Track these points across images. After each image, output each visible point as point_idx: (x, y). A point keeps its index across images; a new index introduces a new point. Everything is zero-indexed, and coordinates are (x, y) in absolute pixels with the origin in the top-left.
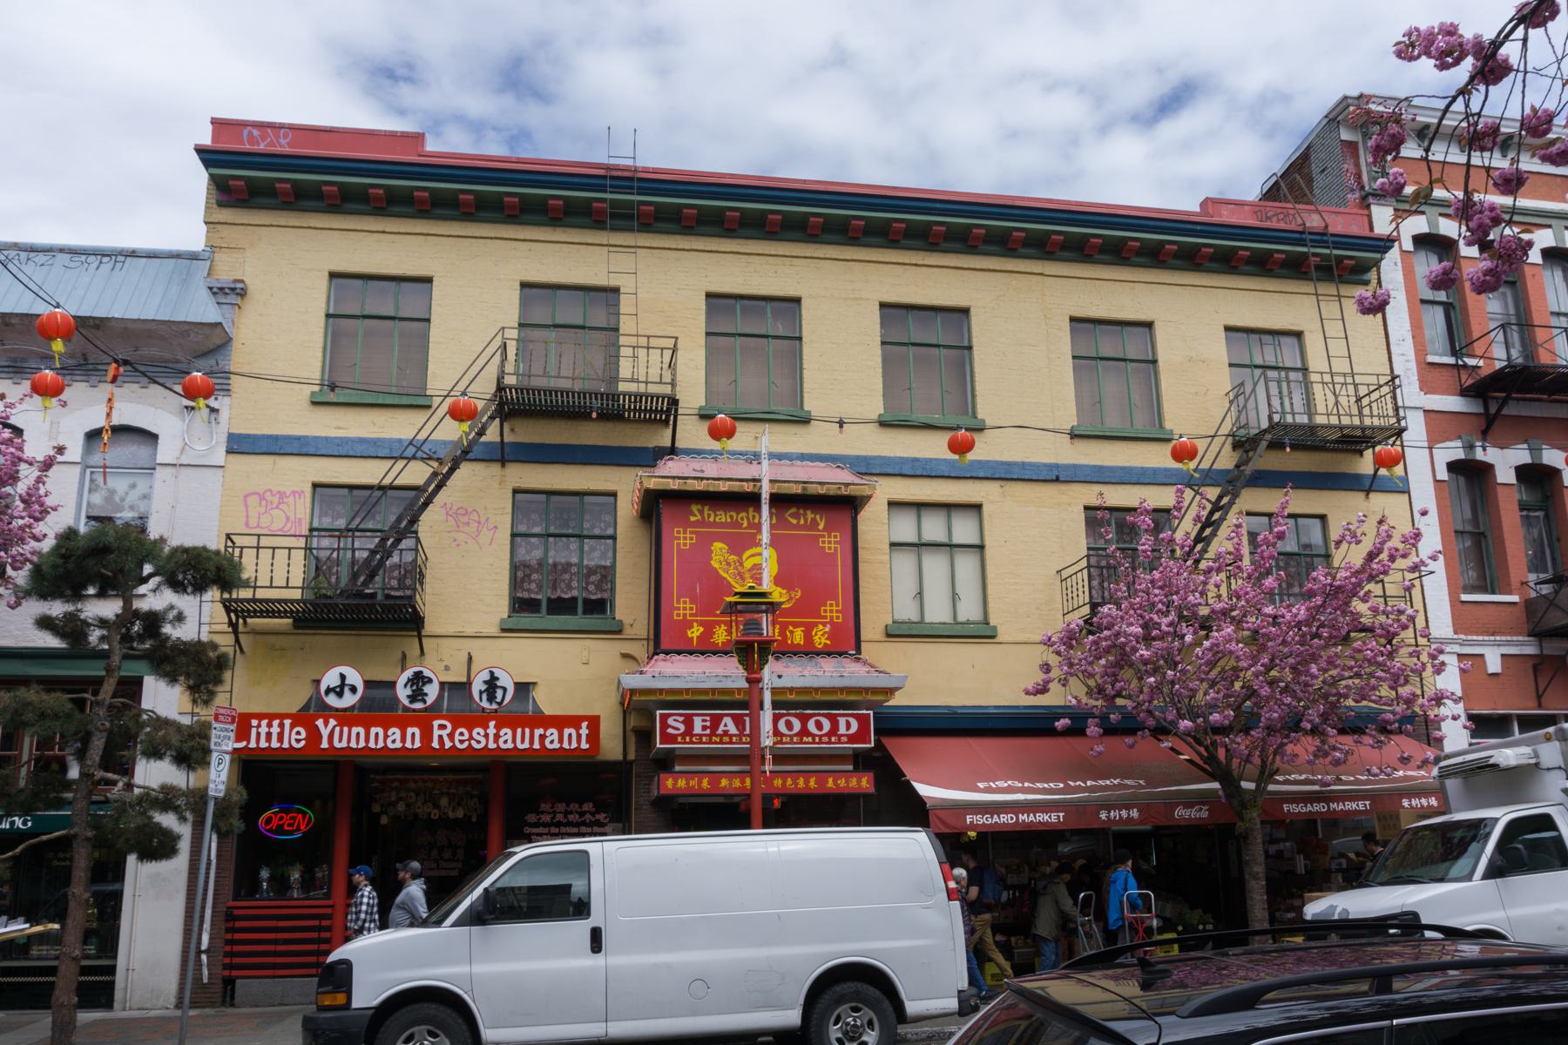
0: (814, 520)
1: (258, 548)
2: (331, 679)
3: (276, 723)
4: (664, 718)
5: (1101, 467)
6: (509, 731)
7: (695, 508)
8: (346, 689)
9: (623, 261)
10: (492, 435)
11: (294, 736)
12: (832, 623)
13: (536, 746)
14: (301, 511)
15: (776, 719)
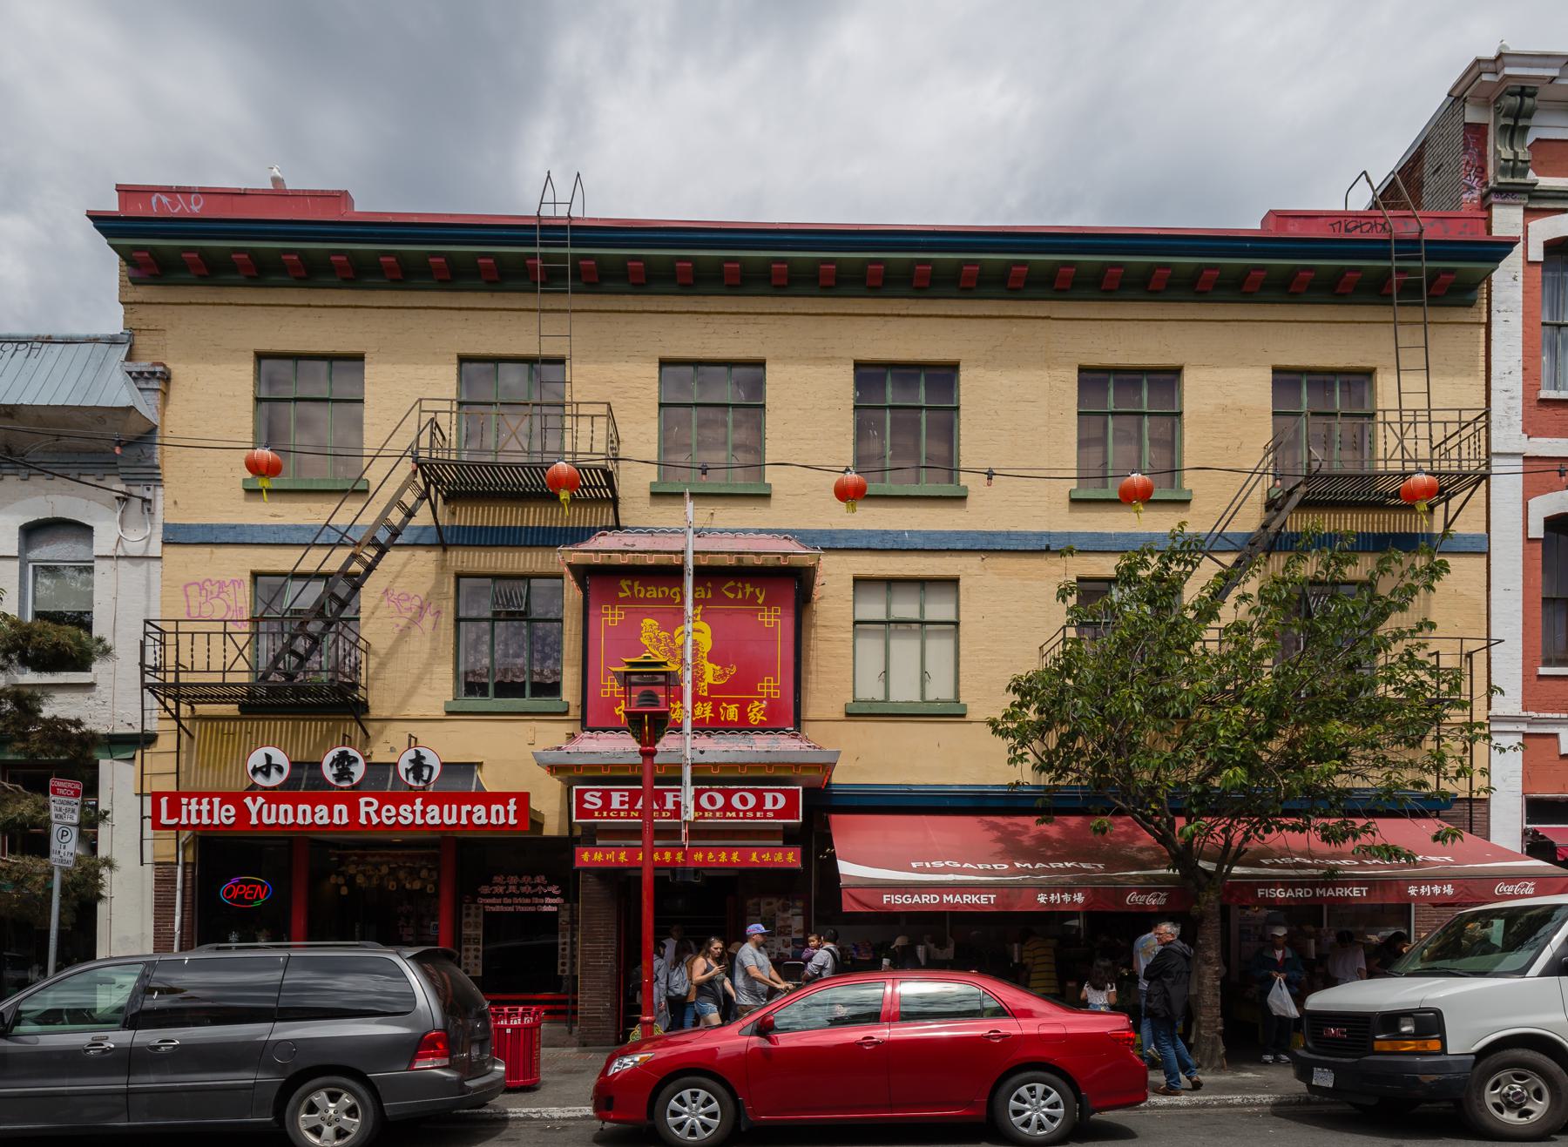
0: (753, 595)
1: (177, 633)
2: (257, 759)
3: (205, 801)
4: (581, 793)
5: (1101, 534)
6: (436, 808)
7: (624, 584)
8: (273, 770)
9: (552, 324)
10: (423, 517)
11: (223, 813)
12: (769, 699)
13: (464, 821)
14: (241, 600)
15: (698, 794)
